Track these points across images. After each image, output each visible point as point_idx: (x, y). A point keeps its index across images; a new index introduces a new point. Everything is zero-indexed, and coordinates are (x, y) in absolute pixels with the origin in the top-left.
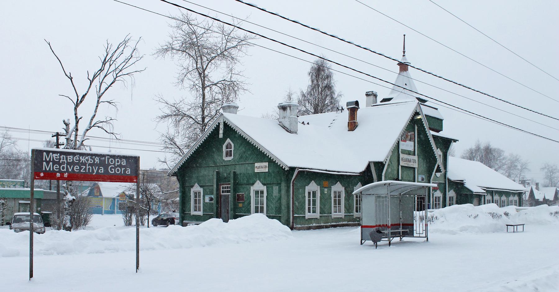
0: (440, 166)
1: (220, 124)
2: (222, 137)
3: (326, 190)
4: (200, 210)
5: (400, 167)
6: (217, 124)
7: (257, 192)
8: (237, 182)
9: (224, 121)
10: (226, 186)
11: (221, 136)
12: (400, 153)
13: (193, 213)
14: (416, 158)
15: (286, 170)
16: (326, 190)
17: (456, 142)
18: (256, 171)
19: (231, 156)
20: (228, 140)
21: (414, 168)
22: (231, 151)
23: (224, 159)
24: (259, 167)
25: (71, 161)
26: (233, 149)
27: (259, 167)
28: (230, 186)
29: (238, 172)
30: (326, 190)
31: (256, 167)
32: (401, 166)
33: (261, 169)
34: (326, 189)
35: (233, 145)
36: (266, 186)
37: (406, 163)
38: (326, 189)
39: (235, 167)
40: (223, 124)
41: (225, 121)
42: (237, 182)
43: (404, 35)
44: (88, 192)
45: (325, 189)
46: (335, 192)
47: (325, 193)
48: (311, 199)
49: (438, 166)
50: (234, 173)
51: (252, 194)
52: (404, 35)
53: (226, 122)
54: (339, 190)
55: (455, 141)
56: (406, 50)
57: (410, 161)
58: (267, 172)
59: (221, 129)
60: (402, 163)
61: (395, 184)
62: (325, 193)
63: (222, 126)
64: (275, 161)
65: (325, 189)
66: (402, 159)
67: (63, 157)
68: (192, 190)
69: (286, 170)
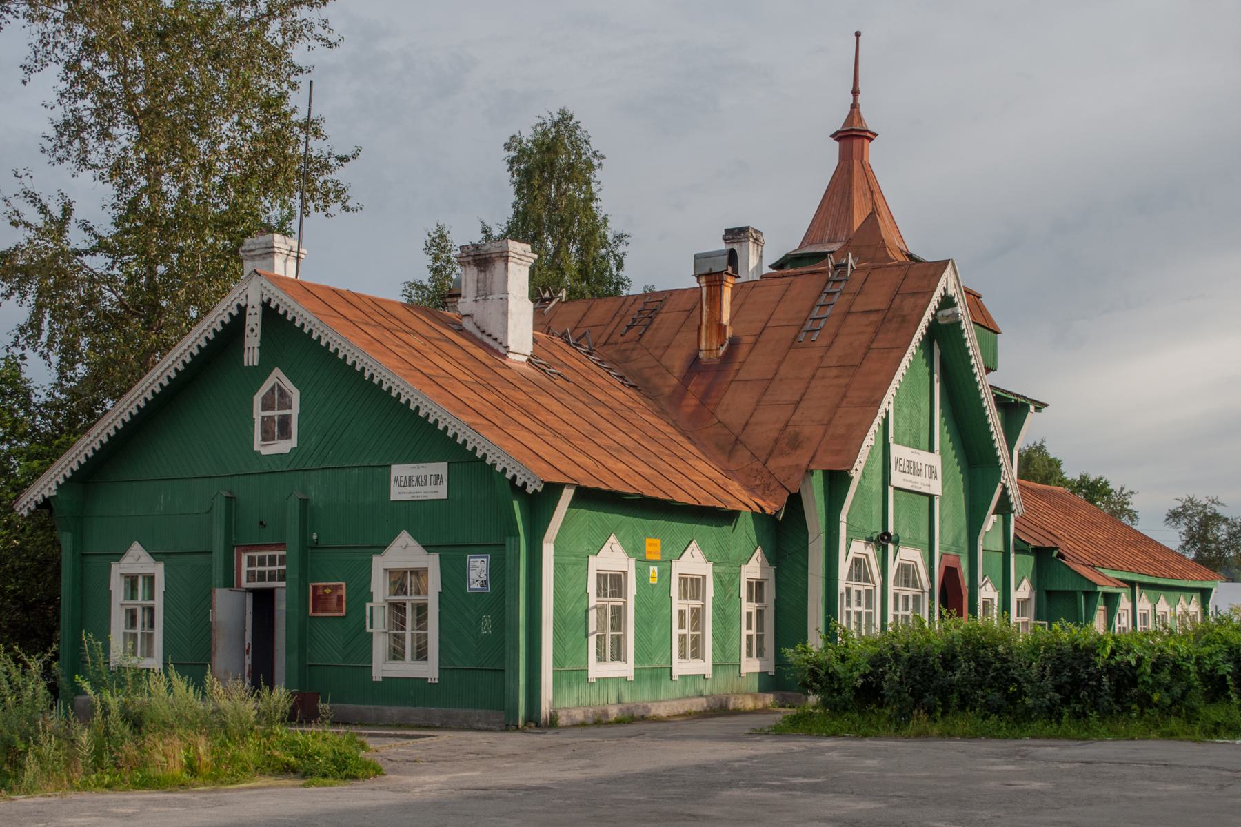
0: (1010, 492)
1: (249, 310)
2: (256, 363)
3: (654, 571)
4: (421, 654)
5: (891, 490)
6: (235, 312)
7: (132, 581)
8: (315, 537)
9: (265, 300)
10: (267, 554)
11: (252, 356)
12: (891, 441)
13: (382, 667)
14: (935, 460)
15: (530, 490)
16: (654, 570)
17: (1040, 412)
18: (397, 493)
19: (290, 437)
20: (278, 377)
21: (931, 497)
22: (288, 417)
23: (255, 449)
24: (410, 481)
26: (295, 411)
27: (410, 481)
28: (284, 553)
29: (315, 495)
30: (654, 570)
31: (396, 481)
32: (896, 488)
33: (418, 488)
34: (656, 568)
35: (295, 396)
36: (437, 556)
37: (908, 476)
38: (656, 568)
39: (784, 481)
40: (259, 309)
41: (270, 300)
42: (315, 537)
43: (858, 34)
44: (1028, 588)
45: (651, 568)
46: (683, 580)
47: (651, 582)
49: (1005, 489)
50: (304, 502)
51: (380, 588)
52: (858, 34)
53: (273, 305)
54: (148, 570)
55: (1040, 406)
56: (861, 86)
57: (918, 472)
58: (443, 500)
59: (252, 330)
60: (897, 479)
61: (274, 547)
62: (651, 582)
63: (254, 321)
64: (485, 456)
65: (651, 568)
66: (897, 463)
68: (118, 572)
69: (530, 490)
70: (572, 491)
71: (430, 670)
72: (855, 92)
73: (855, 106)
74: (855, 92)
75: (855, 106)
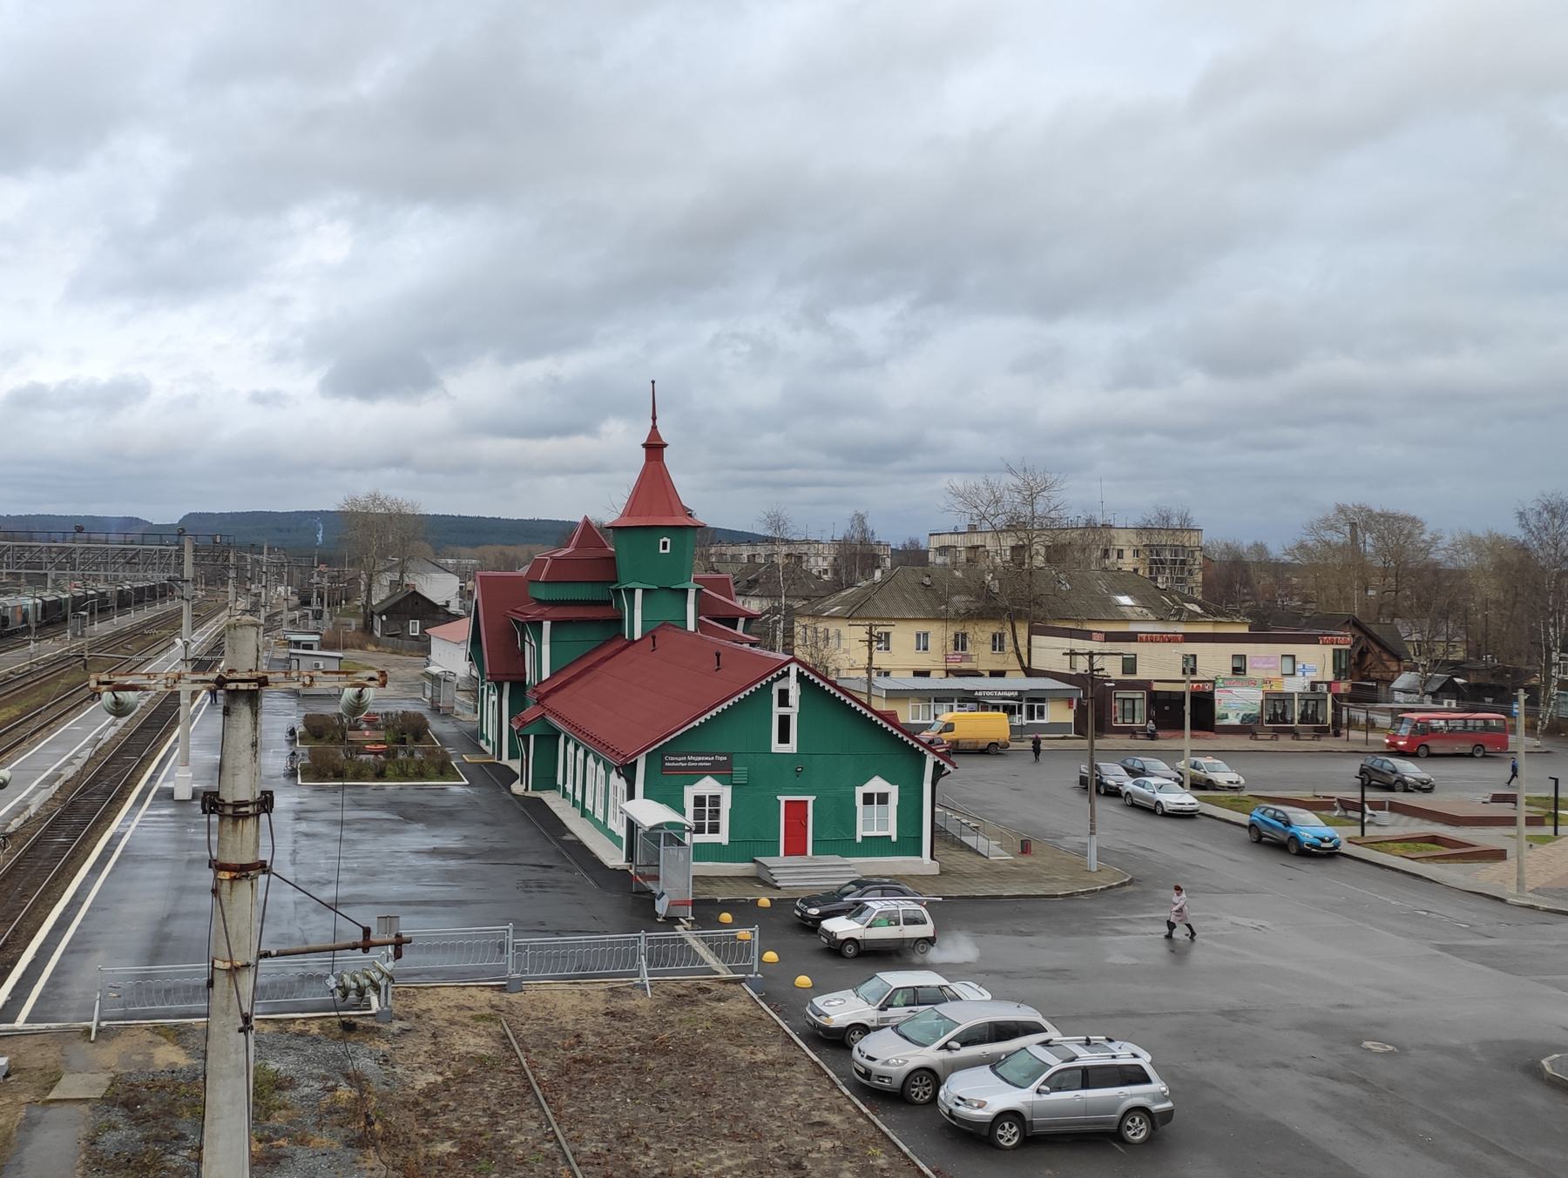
25: (669, 541)
43: (653, 382)
48: (720, 821)
52: (653, 382)
67: (784, 738)
70: (549, 623)
71: (723, 837)
72: (654, 419)
73: (654, 427)
74: (654, 419)
75: (654, 427)
